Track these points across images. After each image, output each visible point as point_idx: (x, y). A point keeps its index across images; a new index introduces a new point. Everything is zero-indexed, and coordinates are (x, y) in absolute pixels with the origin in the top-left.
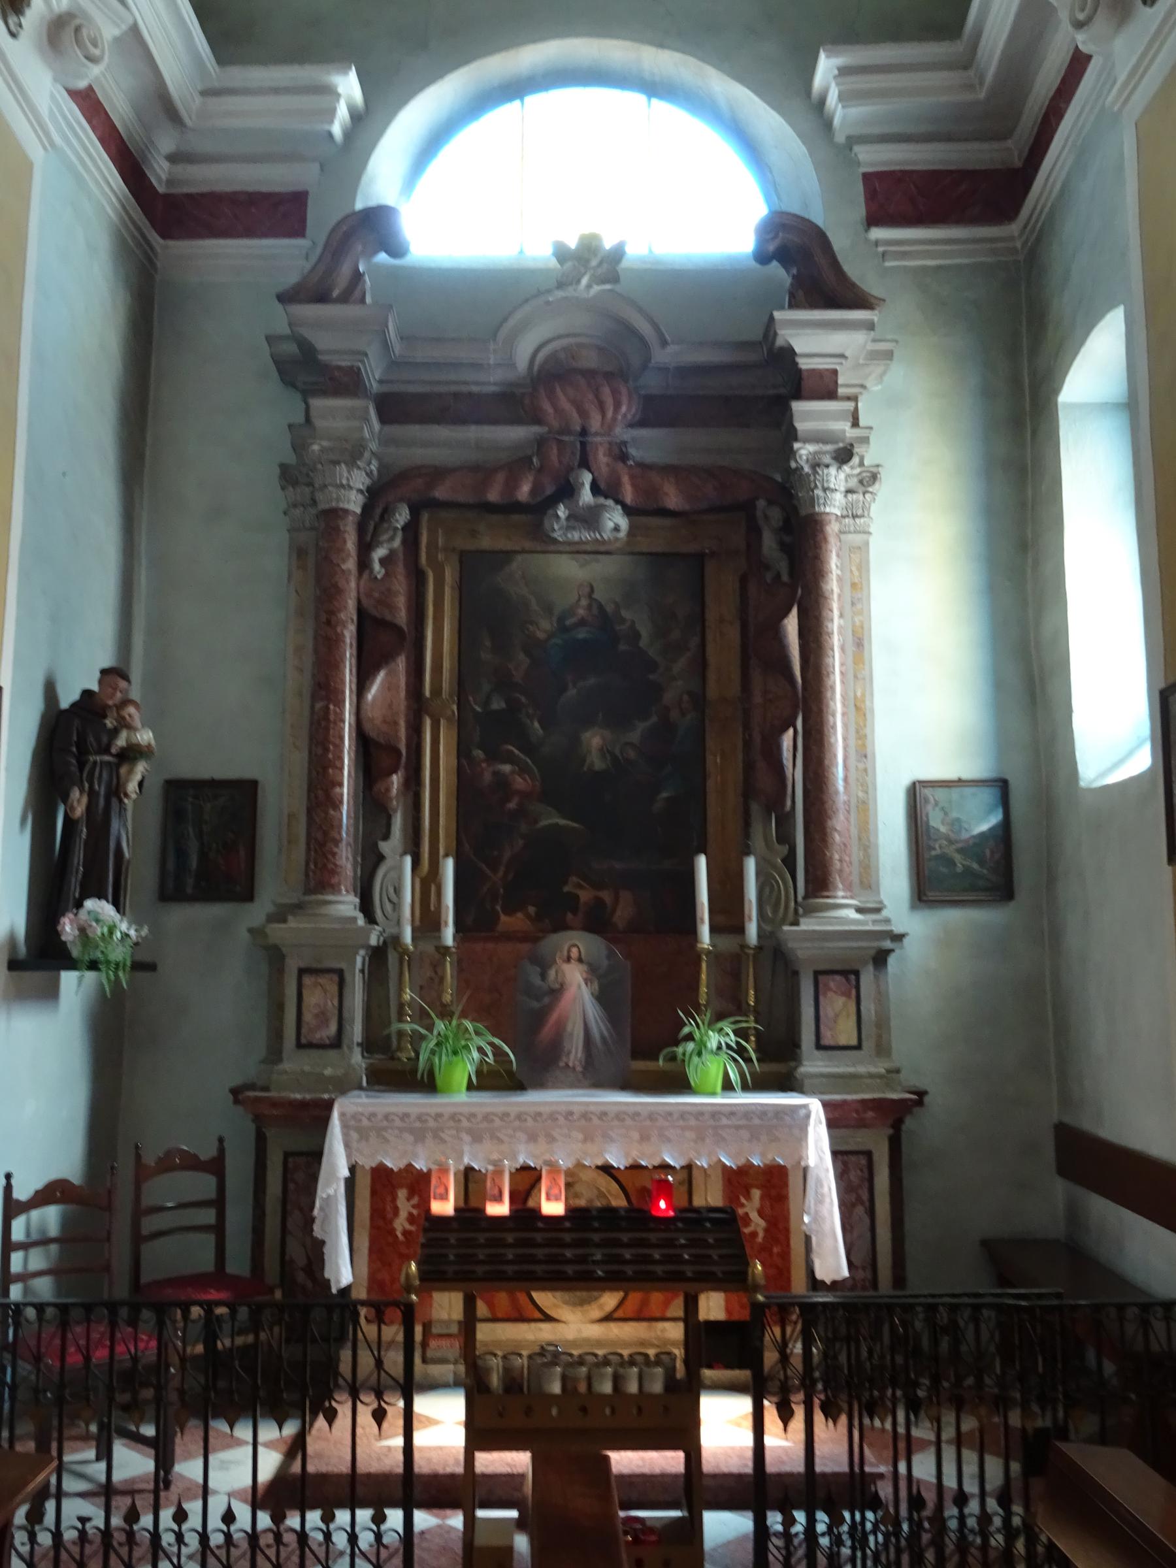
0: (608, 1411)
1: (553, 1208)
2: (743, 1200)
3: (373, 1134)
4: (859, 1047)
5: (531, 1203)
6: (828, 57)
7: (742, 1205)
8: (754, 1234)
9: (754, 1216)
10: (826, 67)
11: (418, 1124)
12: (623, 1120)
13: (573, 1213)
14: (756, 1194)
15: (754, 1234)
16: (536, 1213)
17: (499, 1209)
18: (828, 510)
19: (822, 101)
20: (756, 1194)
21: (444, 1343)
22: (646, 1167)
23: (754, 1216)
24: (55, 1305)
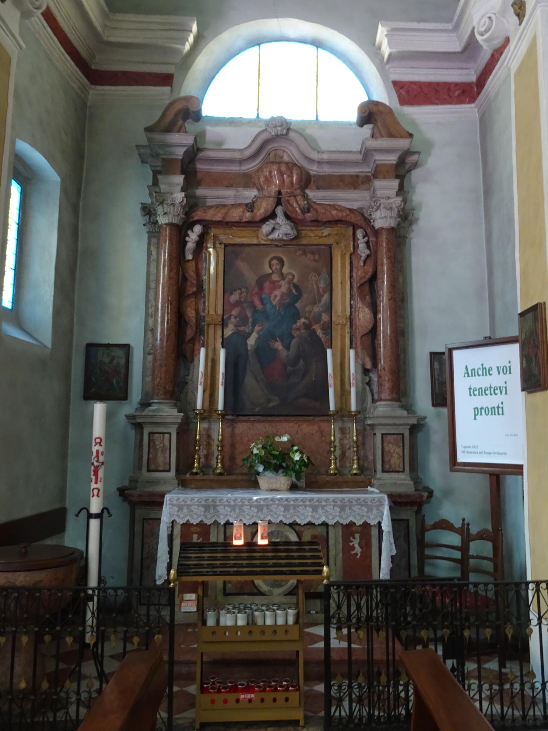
0: (227, 633)
1: (262, 542)
2: (351, 539)
3: (185, 508)
4: (403, 471)
5: (254, 540)
6: (382, 26)
7: (352, 542)
8: (356, 554)
9: (357, 546)
10: (382, 32)
11: (286, 503)
12: (274, 501)
13: (271, 543)
14: (357, 536)
15: (356, 554)
16: (256, 544)
17: (238, 542)
18: (183, 216)
19: (379, 48)
20: (357, 536)
21: (190, 603)
22: (300, 525)
23: (357, 546)
24: (492, 583)
